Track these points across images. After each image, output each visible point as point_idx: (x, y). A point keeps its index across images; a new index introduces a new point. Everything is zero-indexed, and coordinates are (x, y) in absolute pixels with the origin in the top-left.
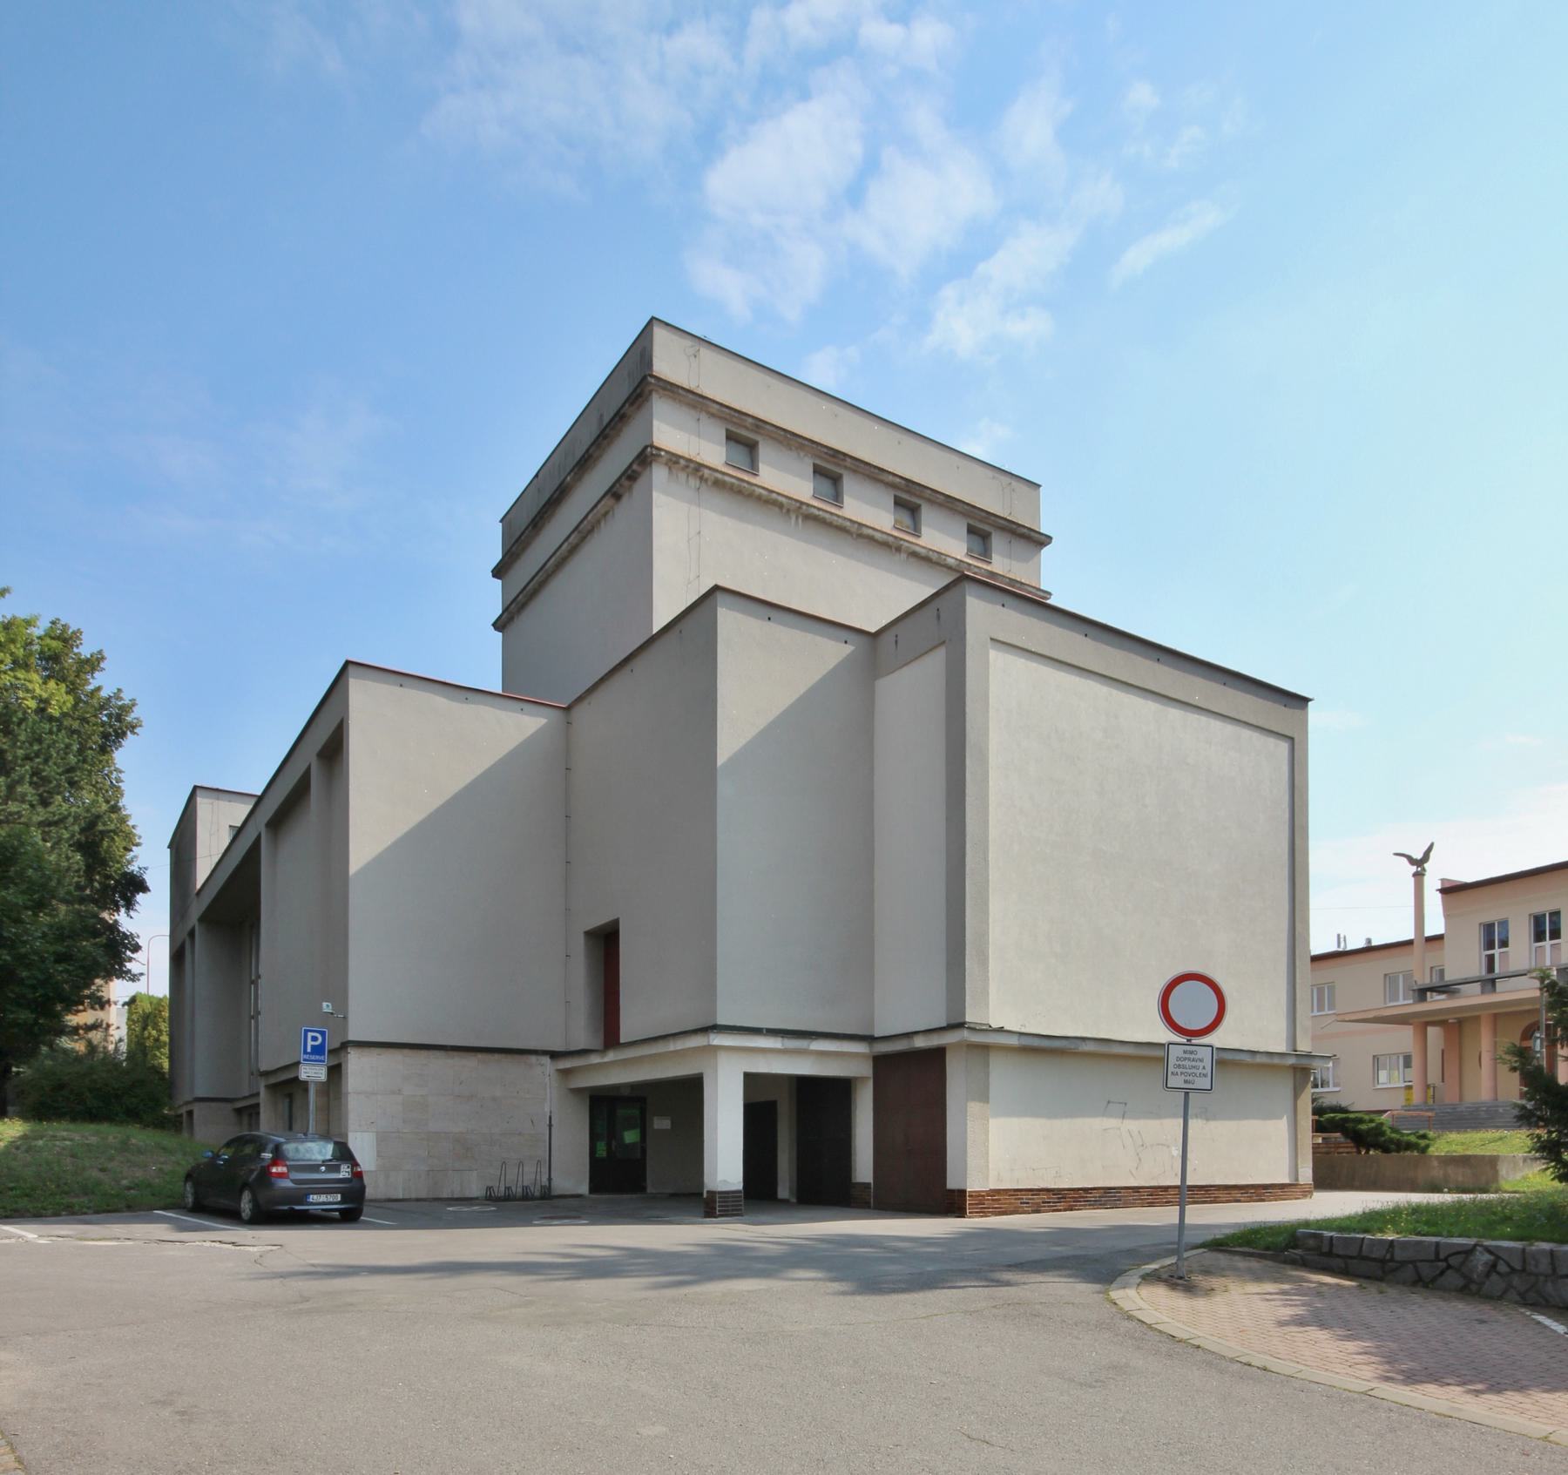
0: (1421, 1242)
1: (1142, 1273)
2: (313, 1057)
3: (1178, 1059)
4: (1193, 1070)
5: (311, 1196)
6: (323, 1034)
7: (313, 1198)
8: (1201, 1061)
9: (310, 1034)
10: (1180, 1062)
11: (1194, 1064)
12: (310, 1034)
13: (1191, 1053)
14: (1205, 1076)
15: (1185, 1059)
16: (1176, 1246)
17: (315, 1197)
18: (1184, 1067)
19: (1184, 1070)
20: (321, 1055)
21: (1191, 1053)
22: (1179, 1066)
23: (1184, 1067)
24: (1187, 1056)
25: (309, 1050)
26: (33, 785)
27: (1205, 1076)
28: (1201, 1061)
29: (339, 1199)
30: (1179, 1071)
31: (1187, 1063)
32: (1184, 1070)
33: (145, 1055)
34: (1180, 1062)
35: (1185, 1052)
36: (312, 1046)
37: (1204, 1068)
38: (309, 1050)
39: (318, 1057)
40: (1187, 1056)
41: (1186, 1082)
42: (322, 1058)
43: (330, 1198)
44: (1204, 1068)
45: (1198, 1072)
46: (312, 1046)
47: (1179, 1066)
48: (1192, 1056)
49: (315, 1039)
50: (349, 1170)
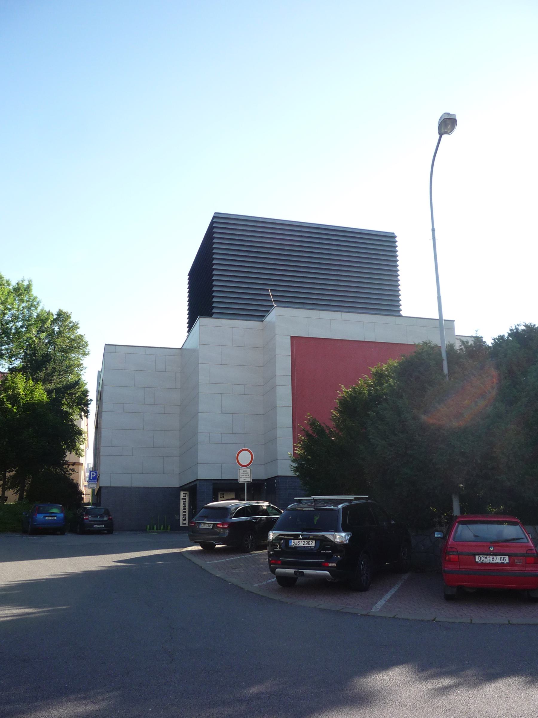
0: (268, 517)
1: (44, 515)
2: (92, 481)
3: (242, 473)
4: (246, 476)
5: (95, 525)
6: (96, 473)
7: (96, 526)
8: (248, 473)
9: (92, 473)
10: (242, 474)
11: (246, 474)
12: (92, 473)
13: (245, 471)
14: (249, 477)
15: (244, 473)
16: (184, 520)
17: (96, 526)
18: (243, 475)
19: (243, 477)
20: (95, 480)
21: (245, 471)
22: (242, 475)
23: (243, 475)
24: (244, 472)
25: (91, 478)
26: (75, 384)
27: (249, 477)
28: (248, 473)
29: (104, 526)
30: (242, 477)
31: (244, 474)
32: (243, 477)
33: (314, 501)
34: (242, 474)
35: (244, 471)
36: (92, 477)
37: (249, 475)
38: (91, 478)
39: (94, 481)
40: (244, 472)
41: (244, 480)
42: (95, 481)
43: (101, 526)
44: (249, 475)
45: (247, 477)
46: (92, 477)
47: (242, 475)
48: (245, 472)
49: (93, 474)
50: (107, 517)
